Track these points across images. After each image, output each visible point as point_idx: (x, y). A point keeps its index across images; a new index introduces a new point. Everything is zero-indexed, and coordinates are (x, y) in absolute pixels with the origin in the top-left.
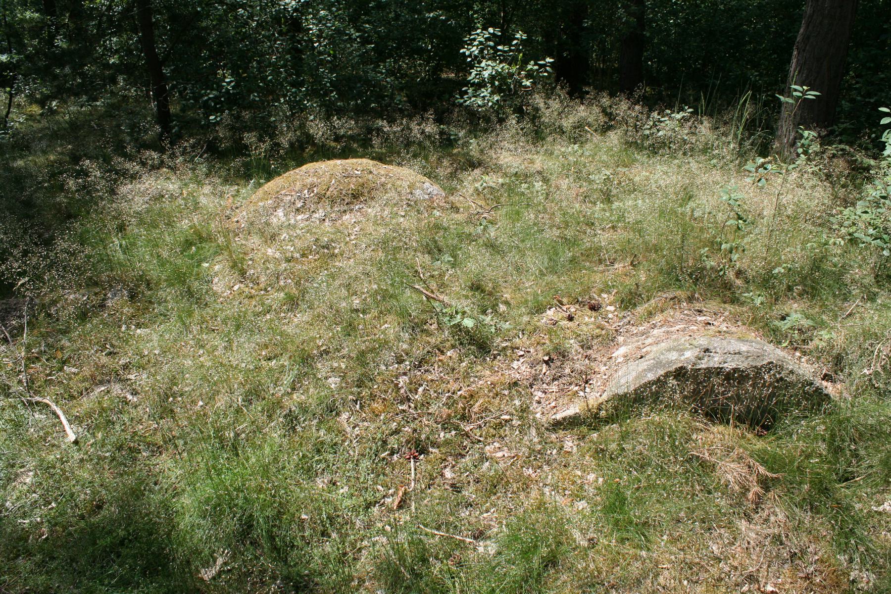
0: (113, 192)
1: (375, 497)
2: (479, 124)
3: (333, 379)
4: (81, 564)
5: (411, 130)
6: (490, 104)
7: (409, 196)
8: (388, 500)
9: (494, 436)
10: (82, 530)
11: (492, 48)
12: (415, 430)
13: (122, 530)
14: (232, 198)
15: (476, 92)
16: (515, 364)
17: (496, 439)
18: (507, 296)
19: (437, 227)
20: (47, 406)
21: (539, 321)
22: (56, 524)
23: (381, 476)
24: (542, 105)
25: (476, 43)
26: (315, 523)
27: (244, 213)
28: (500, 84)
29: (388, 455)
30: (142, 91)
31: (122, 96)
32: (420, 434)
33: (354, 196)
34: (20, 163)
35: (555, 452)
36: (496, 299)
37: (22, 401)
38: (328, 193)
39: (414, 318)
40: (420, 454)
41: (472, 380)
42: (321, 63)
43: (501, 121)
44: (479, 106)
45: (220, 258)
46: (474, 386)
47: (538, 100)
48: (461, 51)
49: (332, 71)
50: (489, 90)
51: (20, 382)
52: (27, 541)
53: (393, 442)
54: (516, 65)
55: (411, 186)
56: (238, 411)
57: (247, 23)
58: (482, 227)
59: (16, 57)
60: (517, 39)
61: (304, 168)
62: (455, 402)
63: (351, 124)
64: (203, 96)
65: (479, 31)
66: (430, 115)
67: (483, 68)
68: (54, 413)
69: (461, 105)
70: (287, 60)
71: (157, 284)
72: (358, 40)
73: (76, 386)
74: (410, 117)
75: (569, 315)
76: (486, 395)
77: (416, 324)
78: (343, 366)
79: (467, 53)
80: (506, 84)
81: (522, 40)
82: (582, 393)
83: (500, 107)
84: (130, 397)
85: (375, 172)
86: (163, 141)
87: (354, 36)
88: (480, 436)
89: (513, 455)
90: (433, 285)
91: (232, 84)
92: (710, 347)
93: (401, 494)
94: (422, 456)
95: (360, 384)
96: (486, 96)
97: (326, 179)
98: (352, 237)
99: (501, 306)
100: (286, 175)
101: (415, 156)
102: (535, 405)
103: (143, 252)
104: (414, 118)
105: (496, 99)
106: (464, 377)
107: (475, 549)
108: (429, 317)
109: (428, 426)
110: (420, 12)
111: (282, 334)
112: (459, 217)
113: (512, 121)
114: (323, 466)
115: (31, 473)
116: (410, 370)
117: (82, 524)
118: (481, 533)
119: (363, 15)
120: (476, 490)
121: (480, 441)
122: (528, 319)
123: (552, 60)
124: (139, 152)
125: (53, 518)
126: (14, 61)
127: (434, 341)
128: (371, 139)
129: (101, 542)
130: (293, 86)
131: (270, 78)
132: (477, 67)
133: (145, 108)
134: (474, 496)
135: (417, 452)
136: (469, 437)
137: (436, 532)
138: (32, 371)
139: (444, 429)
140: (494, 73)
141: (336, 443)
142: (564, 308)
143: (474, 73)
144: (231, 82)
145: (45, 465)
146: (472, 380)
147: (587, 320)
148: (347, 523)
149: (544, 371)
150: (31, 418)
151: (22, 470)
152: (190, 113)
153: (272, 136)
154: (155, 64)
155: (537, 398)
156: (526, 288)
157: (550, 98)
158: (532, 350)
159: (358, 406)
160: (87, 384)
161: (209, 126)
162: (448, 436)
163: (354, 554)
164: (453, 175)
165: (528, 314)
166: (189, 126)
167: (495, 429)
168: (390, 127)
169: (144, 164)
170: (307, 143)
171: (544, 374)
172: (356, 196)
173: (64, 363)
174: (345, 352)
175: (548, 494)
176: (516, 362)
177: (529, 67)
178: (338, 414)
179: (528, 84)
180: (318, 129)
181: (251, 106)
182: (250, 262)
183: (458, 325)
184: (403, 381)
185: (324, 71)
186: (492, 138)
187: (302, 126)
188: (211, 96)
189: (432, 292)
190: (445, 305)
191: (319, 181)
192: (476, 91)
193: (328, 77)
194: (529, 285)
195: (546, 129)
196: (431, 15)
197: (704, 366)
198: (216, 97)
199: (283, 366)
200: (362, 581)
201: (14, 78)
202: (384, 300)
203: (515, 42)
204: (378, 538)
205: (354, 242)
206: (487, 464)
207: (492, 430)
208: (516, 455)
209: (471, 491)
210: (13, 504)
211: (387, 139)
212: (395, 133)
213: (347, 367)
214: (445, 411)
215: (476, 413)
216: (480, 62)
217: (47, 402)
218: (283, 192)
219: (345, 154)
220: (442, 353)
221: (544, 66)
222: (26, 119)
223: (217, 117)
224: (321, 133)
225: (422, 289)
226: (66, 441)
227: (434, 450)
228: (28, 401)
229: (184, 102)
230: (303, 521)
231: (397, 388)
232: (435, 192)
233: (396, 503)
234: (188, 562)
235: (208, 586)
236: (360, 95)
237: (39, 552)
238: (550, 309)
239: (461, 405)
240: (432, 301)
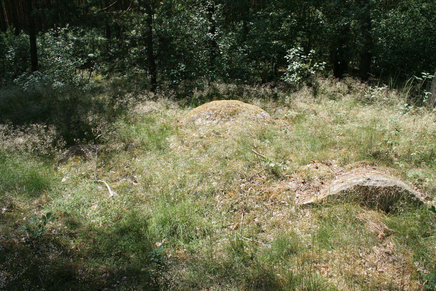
8: (231, 227)
16: (290, 183)
28: (302, 73)
31: (135, 73)
44: (291, 82)
48: (285, 57)
49: (227, 64)
50: (296, 75)
53: (235, 207)
57: (192, 43)
60: (311, 53)
68: (106, 187)
84: (134, 183)
85: (241, 106)
92: (371, 178)
97: (220, 107)
102: (296, 198)
113: (305, 88)
116: (246, 182)
123: (325, 63)
126: (96, 56)
143: (289, 67)
144: (184, 67)
147: (323, 170)
149: (302, 186)
154: (152, 58)
155: (297, 196)
158: (298, 178)
159: (223, 193)
173: (110, 169)
177: (315, 65)
179: (313, 73)
192: (290, 75)
194: (302, 155)
196: (275, 42)
197: (366, 185)
203: (309, 54)
216: (292, 62)
217: (103, 181)
219: (229, 99)
222: (95, 82)
223: (177, 81)
232: (266, 116)
238: (309, 164)
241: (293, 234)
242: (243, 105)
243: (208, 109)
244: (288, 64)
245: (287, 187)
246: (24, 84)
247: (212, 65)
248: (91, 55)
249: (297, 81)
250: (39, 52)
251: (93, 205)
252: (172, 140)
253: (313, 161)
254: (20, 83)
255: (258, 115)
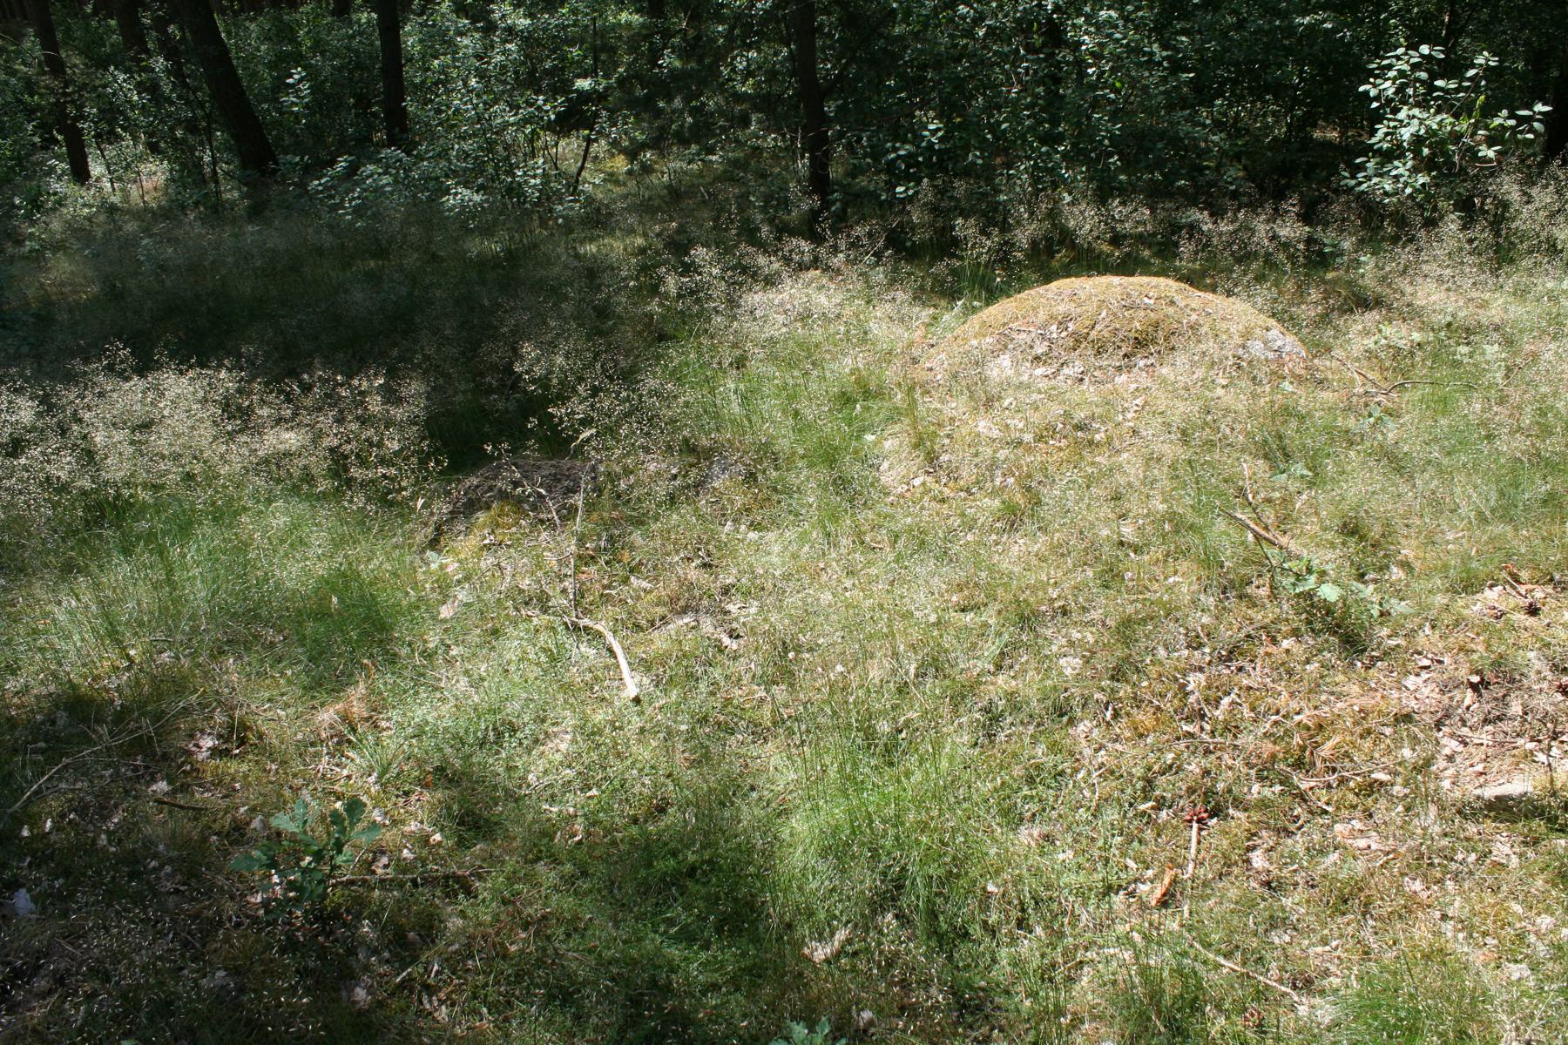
0: (732, 303)
1: (1119, 878)
2: (1381, 227)
3: (1069, 659)
4: (627, 893)
5: (1253, 231)
6: (1409, 191)
7: (1241, 351)
8: (1143, 888)
9: (1354, 807)
10: (632, 841)
11: (1423, 82)
12: (1207, 772)
13: (693, 853)
14: (923, 328)
15: (1383, 167)
16: (1411, 681)
17: (1358, 814)
18: (1407, 552)
19: (1287, 412)
20: (600, 635)
21: (1467, 606)
22: (594, 824)
23: (1136, 844)
24: (1515, 196)
25: (1392, 74)
26: (1009, 903)
27: (943, 356)
29: (1152, 808)
30: (784, 139)
32: (1215, 780)
33: (1139, 343)
34: (591, 248)
35: (1473, 857)
36: (1386, 556)
37: (566, 623)
38: (1094, 334)
39: (1228, 572)
40: (1211, 817)
41: (1323, 697)
42: (1096, 104)
43: (1430, 223)
44: (1386, 194)
45: (897, 428)
46: (1327, 709)
47: (1509, 187)
48: (1361, 89)
49: (1114, 117)
50: (1410, 164)
51: (564, 591)
52: (552, 839)
54: (1470, 118)
55: (1247, 334)
56: (902, 690)
58: (1372, 420)
59: (604, 83)
61: (1054, 285)
62: (1288, 733)
63: (1143, 214)
64: (888, 152)
65: (1401, 51)
66: (1292, 205)
67: (1401, 121)
68: (610, 650)
69: (1350, 189)
70: (1036, 96)
71: (790, 460)
72: (1165, 64)
73: (646, 610)
74: (1254, 206)
75: (1531, 605)
76: (1346, 729)
77: (1231, 581)
78: (1091, 639)
79: (1373, 93)
80: (1445, 153)
81: (1488, 69)
82: (1542, 757)
83: (1429, 198)
84: (726, 641)
85: (1182, 304)
86: (819, 222)
87: (1157, 58)
88: (1328, 804)
89: (1387, 849)
90: (1270, 516)
91: (940, 134)
93: (1167, 881)
94: (1215, 820)
95: (1117, 675)
96: (1402, 176)
97: (1091, 308)
98: (1129, 416)
99: (1394, 569)
100: (1022, 295)
101: (1260, 278)
103: (770, 406)
104: (1259, 210)
105: (1421, 181)
106: (1310, 692)
107: (1293, 1008)
108: (1255, 574)
109: (1230, 768)
110: (1284, 15)
111: (991, 569)
112: (1326, 396)
113: (1452, 224)
114: (1034, 807)
115: (568, 737)
116: (1210, 663)
117: (634, 830)
118: (1309, 982)
119: (1177, 18)
120: (1308, 901)
121: (1326, 812)
122: (1445, 601)
124: (779, 239)
125: (593, 813)
126: (601, 88)
127: (1260, 617)
128: (1178, 242)
129: (659, 865)
130: (1043, 142)
131: (1004, 126)
132: (1389, 120)
133: (786, 168)
134: (1302, 911)
135: (1206, 811)
136: (1305, 801)
137: (1223, 961)
138: (583, 577)
139: (1261, 778)
140: (1422, 132)
141: (1063, 771)
142: (1522, 589)
143: (1382, 130)
144: (938, 129)
145: (588, 729)
146: (1323, 697)
148: (1064, 913)
149: (1467, 702)
150: (575, 650)
151: (555, 729)
152: (862, 182)
153: (1005, 228)
154: (813, 93)
155: (1447, 751)
156: (1448, 542)
157: (1534, 184)
158: (1447, 660)
160: (660, 610)
161: (893, 201)
162: (1267, 792)
163: (1069, 969)
164: (1324, 319)
165: (1448, 591)
166: (858, 203)
167: (1357, 795)
168: (1215, 223)
169: (787, 260)
170: (1061, 243)
171: (1468, 708)
172: (1140, 343)
174: (1096, 615)
175: (1449, 934)
176: (1412, 677)
178: (1072, 722)
179: (1491, 154)
180: (1083, 219)
181: (968, 172)
182: (947, 441)
183: (1309, 595)
184: (1195, 681)
185: (1101, 118)
186: (1405, 255)
187: (1053, 214)
188: (902, 153)
189: (1266, 528)
190: (1290, 556)
191: (1079, 310)
193: (1106, 126)
195: (1522, 242)
198: (910, 155)
199: (986, 625)
200: (1077, 1021)
201: (596, 115)
202: (1177, 532)
203: (1471, 73)
204: (1117, 950)
205: (1131, 424)
206: (1334, 857)
207: (1351, 796)
208: (1394, 851)
209: (1296, 901)
210: (538, 778)
211: (1207, 245)
212: (1221, 235)
213: (1097, 642)
214: (1268, 747)
215: (1324, 760)
216: (1396, 111)
217: (599, 627)
218: (1013, 325)
219: (1126, 267)
220: (1274, 641)
221: (1528, 119)
222: (604, 180)
223: (907, 189)
224: (1088, 227)
225: (1248, 522)
226: (623, 695)
227: (1237, 814)
228: (573, 623)
229: (855, 161)
230: (988, 895)
231: (1183, 692)
232: (1288, 348)
233: (1158, 893)
234: (789, 926)
235: (816, 969)
236: (1158, 164)
237: (569, 861)
238: (1491, 587)
239: (1297, 740)
240: (1264, 543)
241: (1436, 955)
242: (1188, 301)
243: (1042, 316)
244: (1377, 117)
245: (1398, 701)
246: (342, 201)
247: (1055, 122)
248: (584, 84)
249: (1416, 190)
250: (413, 75)
251: (555, 735)
252: (888, 444)
253: (1511, 574)
254: (332, 197)
255: (1256, 347)
